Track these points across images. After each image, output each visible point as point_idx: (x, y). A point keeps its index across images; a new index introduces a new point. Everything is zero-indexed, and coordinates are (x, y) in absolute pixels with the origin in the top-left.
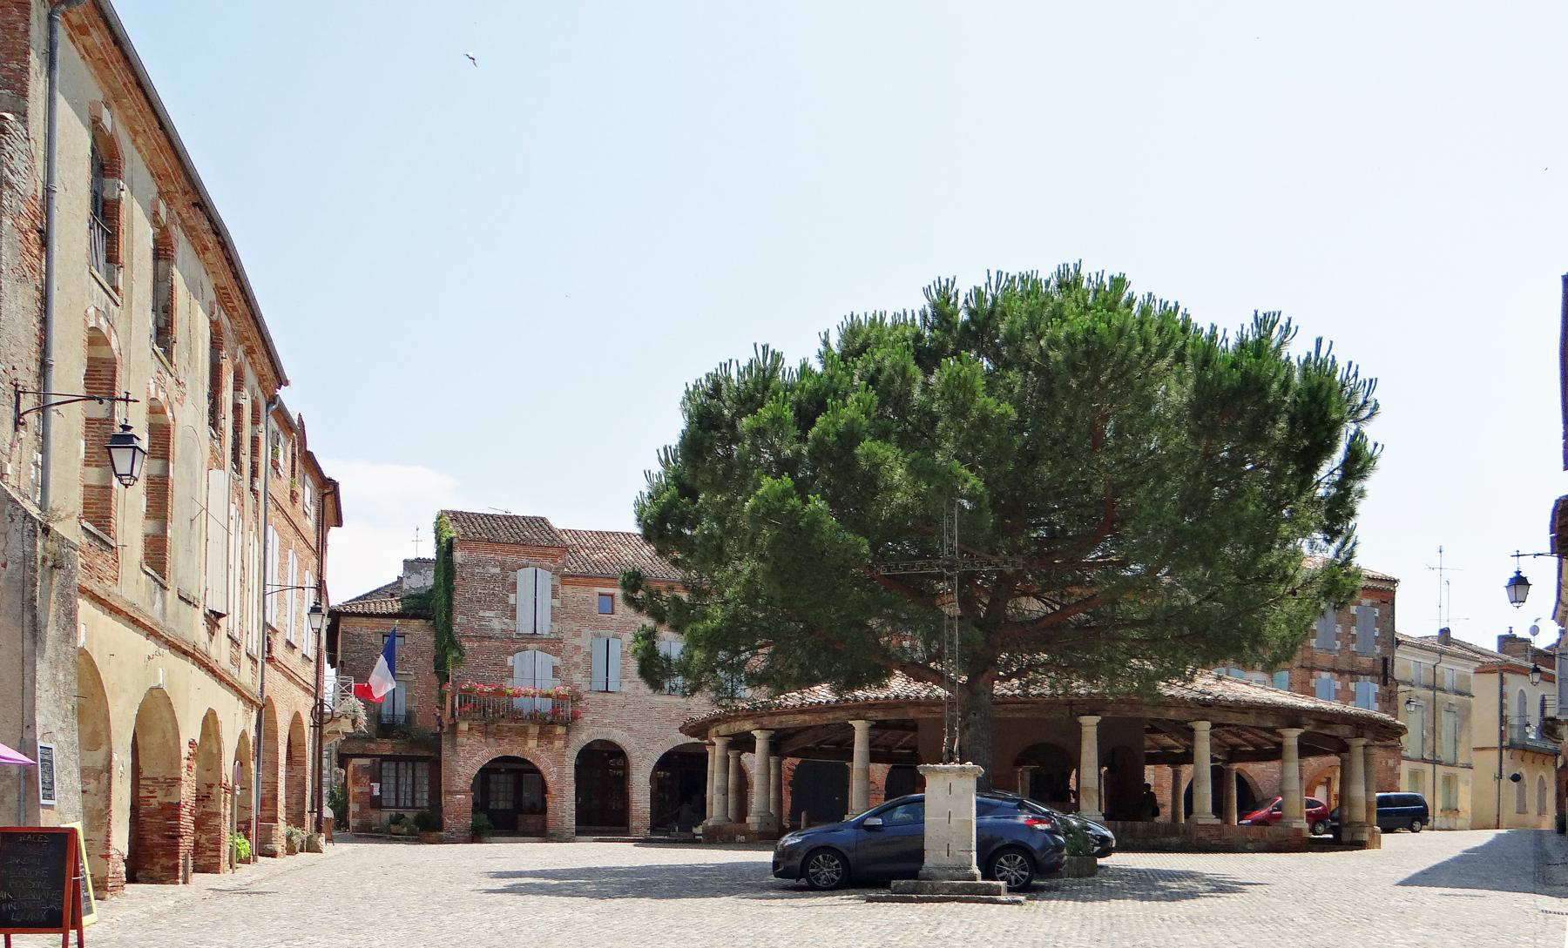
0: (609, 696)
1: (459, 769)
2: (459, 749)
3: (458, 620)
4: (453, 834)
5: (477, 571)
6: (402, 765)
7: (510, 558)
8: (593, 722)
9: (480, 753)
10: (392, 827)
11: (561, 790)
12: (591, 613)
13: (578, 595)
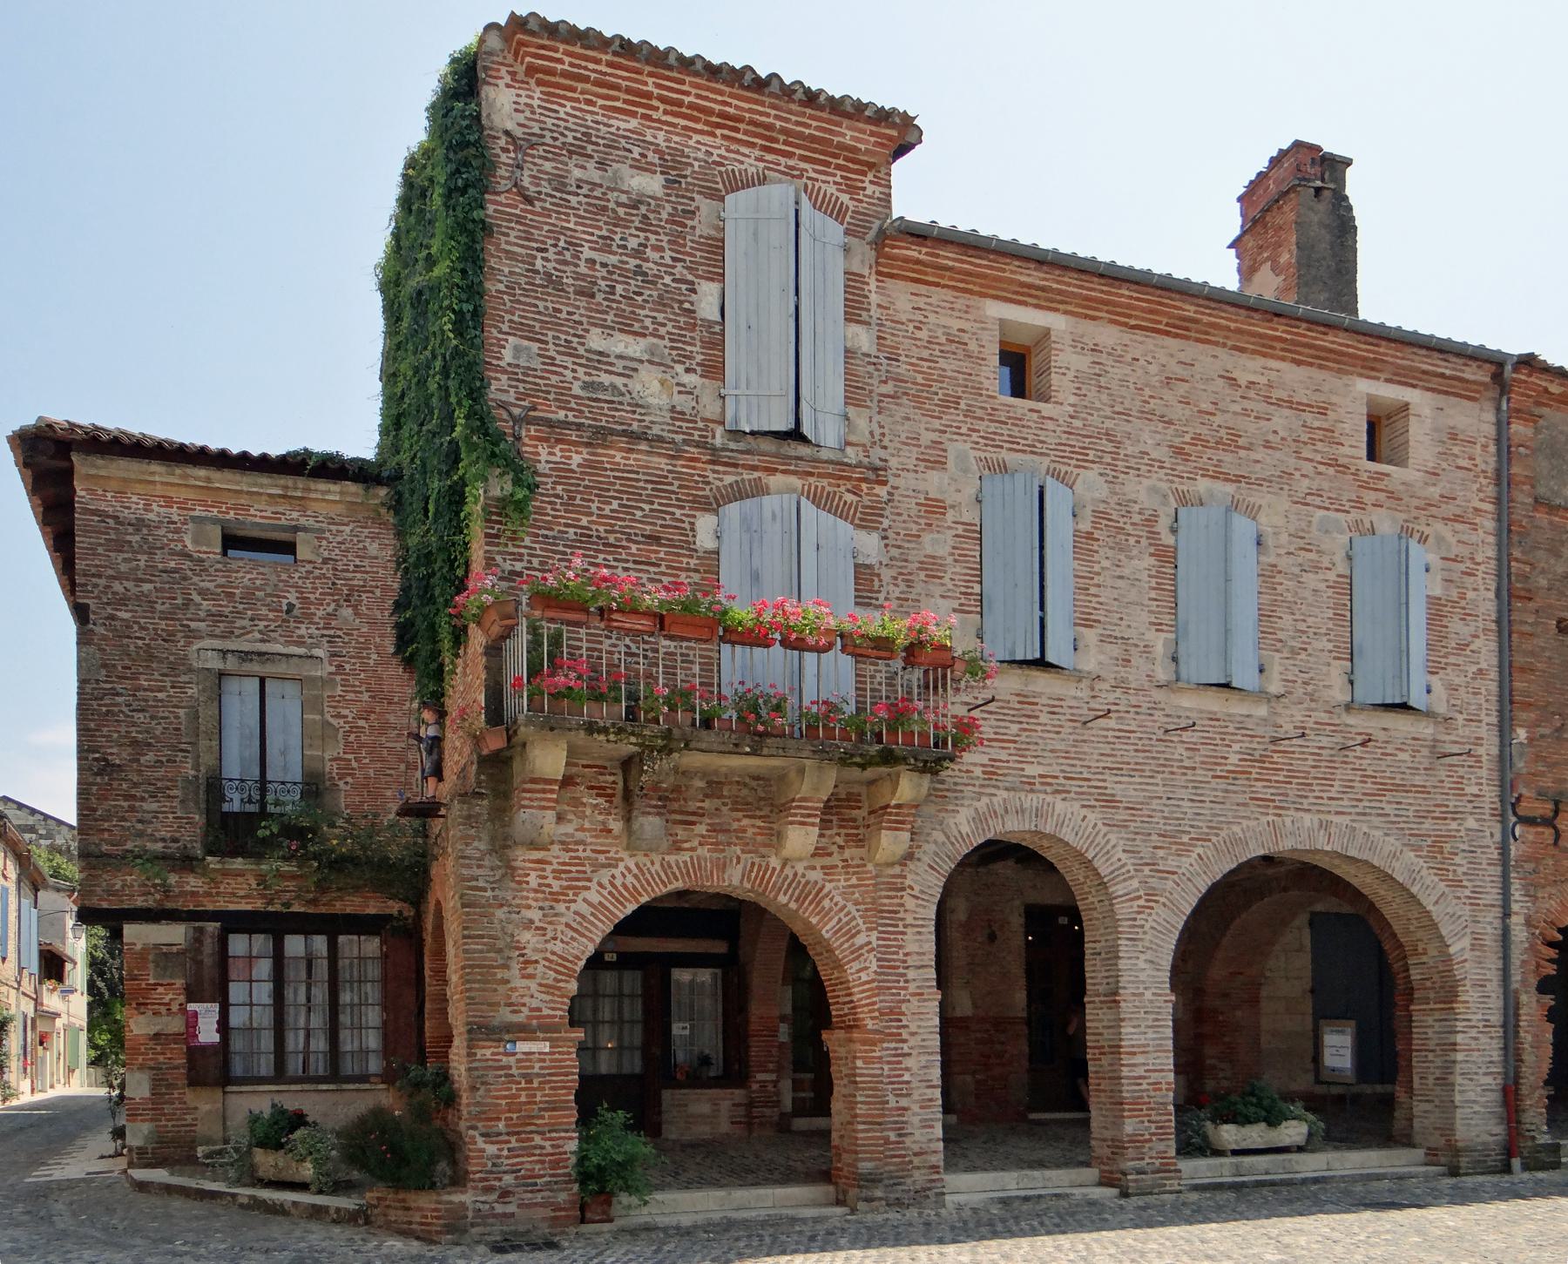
0: (1041, 682)
1: (526, 937)
2: (522, 857)
3: (508, 355)
4: (505, 1194)
5: (577, 173)
7: (702, 147)
8: (991, 773)
9: (604, 876)
11: (894, 1013)
12: (978, 391)
13: (932, 318)
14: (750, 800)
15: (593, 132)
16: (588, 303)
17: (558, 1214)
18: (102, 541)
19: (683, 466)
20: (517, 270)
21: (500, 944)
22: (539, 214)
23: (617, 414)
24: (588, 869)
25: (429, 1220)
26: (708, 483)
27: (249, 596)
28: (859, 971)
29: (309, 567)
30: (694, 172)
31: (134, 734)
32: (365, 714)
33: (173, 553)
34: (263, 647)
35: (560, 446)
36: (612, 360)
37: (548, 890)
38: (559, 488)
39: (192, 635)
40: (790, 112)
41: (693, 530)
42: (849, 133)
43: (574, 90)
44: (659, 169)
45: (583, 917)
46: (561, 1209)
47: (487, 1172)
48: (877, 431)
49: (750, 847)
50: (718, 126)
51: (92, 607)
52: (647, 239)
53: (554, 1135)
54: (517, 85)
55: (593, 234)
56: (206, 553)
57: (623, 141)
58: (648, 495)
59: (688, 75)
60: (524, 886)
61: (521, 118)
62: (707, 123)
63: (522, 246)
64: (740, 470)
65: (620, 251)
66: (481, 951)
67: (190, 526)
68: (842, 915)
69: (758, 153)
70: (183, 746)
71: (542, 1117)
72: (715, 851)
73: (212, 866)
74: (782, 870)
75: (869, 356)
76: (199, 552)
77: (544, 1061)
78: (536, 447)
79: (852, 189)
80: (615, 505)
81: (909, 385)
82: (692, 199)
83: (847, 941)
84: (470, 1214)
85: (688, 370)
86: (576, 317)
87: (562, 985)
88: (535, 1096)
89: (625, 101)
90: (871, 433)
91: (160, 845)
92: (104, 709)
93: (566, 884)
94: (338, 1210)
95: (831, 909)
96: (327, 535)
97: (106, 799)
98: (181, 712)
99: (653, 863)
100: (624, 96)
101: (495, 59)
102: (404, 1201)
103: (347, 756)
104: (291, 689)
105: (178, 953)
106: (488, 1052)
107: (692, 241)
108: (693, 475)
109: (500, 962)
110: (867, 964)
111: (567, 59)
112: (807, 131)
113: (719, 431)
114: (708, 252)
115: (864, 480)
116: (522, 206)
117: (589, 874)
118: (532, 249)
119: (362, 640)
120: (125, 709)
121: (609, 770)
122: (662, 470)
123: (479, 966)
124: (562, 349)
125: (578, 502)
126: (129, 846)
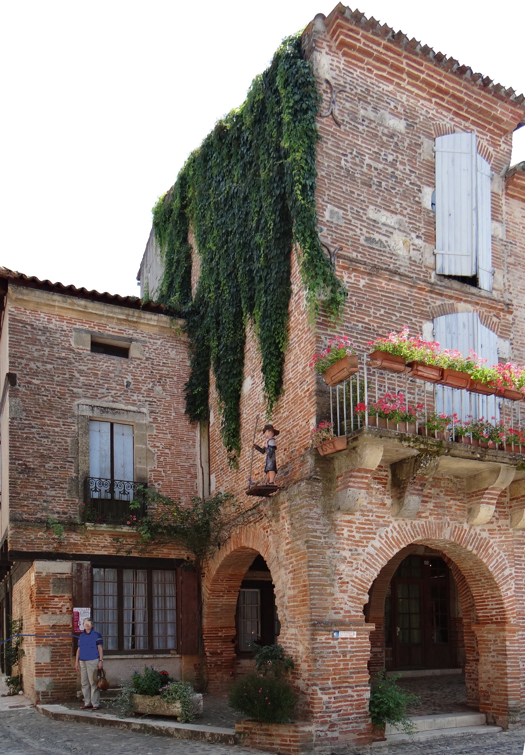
1: (342, 567)
2: (340, 518)
3: (327, 214)
4: (333, 725)
5: (362, 112)
6: (128, 575)
9: (382, 531)
10: (139, 699)
14: (454, 489)
15: (371, 89)
16: (368, 190)
17: (361, 737)
18: (24, 338)
19: (416, 293)
20: (332, 165)
21: (329, 571)
22: (344, 134)
23: (383, 258)
24: (374, 527)
25: (288, 743)
26: (428, 304)
27: (106, 376)
28: (507, 590)
29: (138, 362)
30: (420, 122)
31: (42, 451)
32: (168, 446)
33: (64, 348)
34: (114, 405)
35: (354, 274)
36: (380, 225)
37: (353, 539)
38: (354, 298)
39: (74, 396)
40: (473, 92)
41: (421, 330)
42: (500, 109)
43: (362, 61)
44: (403, 117)
45: (372, 556)
46: (363, 734)
47: (324, 712)
48: (507, 284)
49: (454, 517)
50: (434, 96)
51: (18, 376)
52: (397, 157)
53: (358, 688)
54: (332, 54)
55: (370, 150)
56: (82, 349)
57: (386, 97)
58: (399, 308)
59: (425, 60)
60: (341, 536)
61: (333, 74)
62: (429, 93)
63: (334, 151)
64: (443, 298)
65: (384, 162)
66: (319, 576)
67: (74, 333)
68: (498, 558)
69: (451, 116)
70: (69, 459)
71: (352, 678)
72: (438, 519)
73: (88, 528)
74: (469, 532)
75: (502, 240)
76: (78, 348)
77: (353, 643)
78: (342, 272)
79: (495, 145)
80: (382, 311)
81: (521, 259)
82: (420, 137)
83: (500, 573)
84: (314, 738)
85: (418, 237)
86: (361, 198)
87: (361, 597)
88: (348, 664)
89: (389, 73)
90: (504, 284)
91: (56, 516)
92: (25, 435)
93: (363, 536)
94: (212, 735)
95: (492, 554)
96: (148, 344)
97: (26, 488)
98: (69, 440)
99: (406, 525)
100: (388, 69)
101: (321, 36)
102: (267, 730)
103: (159, 469)
104: (127, 430)
105: (66, 579)
106: (323, 638)
107: (420, 162)
108: (421, 298)
109: (329, 582)
110: (510, 586)
111: (363, 40)
112: (479, 105)
113: (433, 274)
114: (427, 169)
115: (502, 310)
116: (334, 127)
117: (374, 531)
118: (339, 153)
119: (167, 404)
120: (36, 436)
121: (384, 469)
122: (406, 293)
123: (317, 585)
124: (354, 216)
125: (363, 308)
126: (39, 515)
